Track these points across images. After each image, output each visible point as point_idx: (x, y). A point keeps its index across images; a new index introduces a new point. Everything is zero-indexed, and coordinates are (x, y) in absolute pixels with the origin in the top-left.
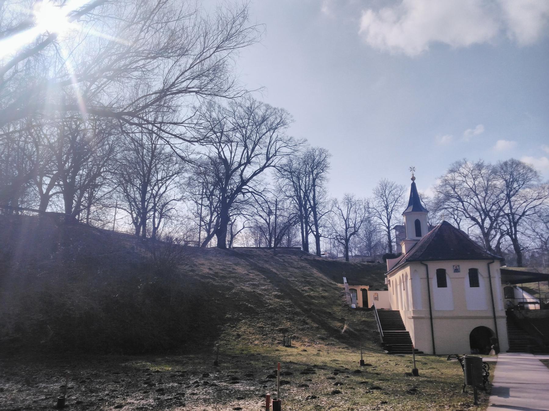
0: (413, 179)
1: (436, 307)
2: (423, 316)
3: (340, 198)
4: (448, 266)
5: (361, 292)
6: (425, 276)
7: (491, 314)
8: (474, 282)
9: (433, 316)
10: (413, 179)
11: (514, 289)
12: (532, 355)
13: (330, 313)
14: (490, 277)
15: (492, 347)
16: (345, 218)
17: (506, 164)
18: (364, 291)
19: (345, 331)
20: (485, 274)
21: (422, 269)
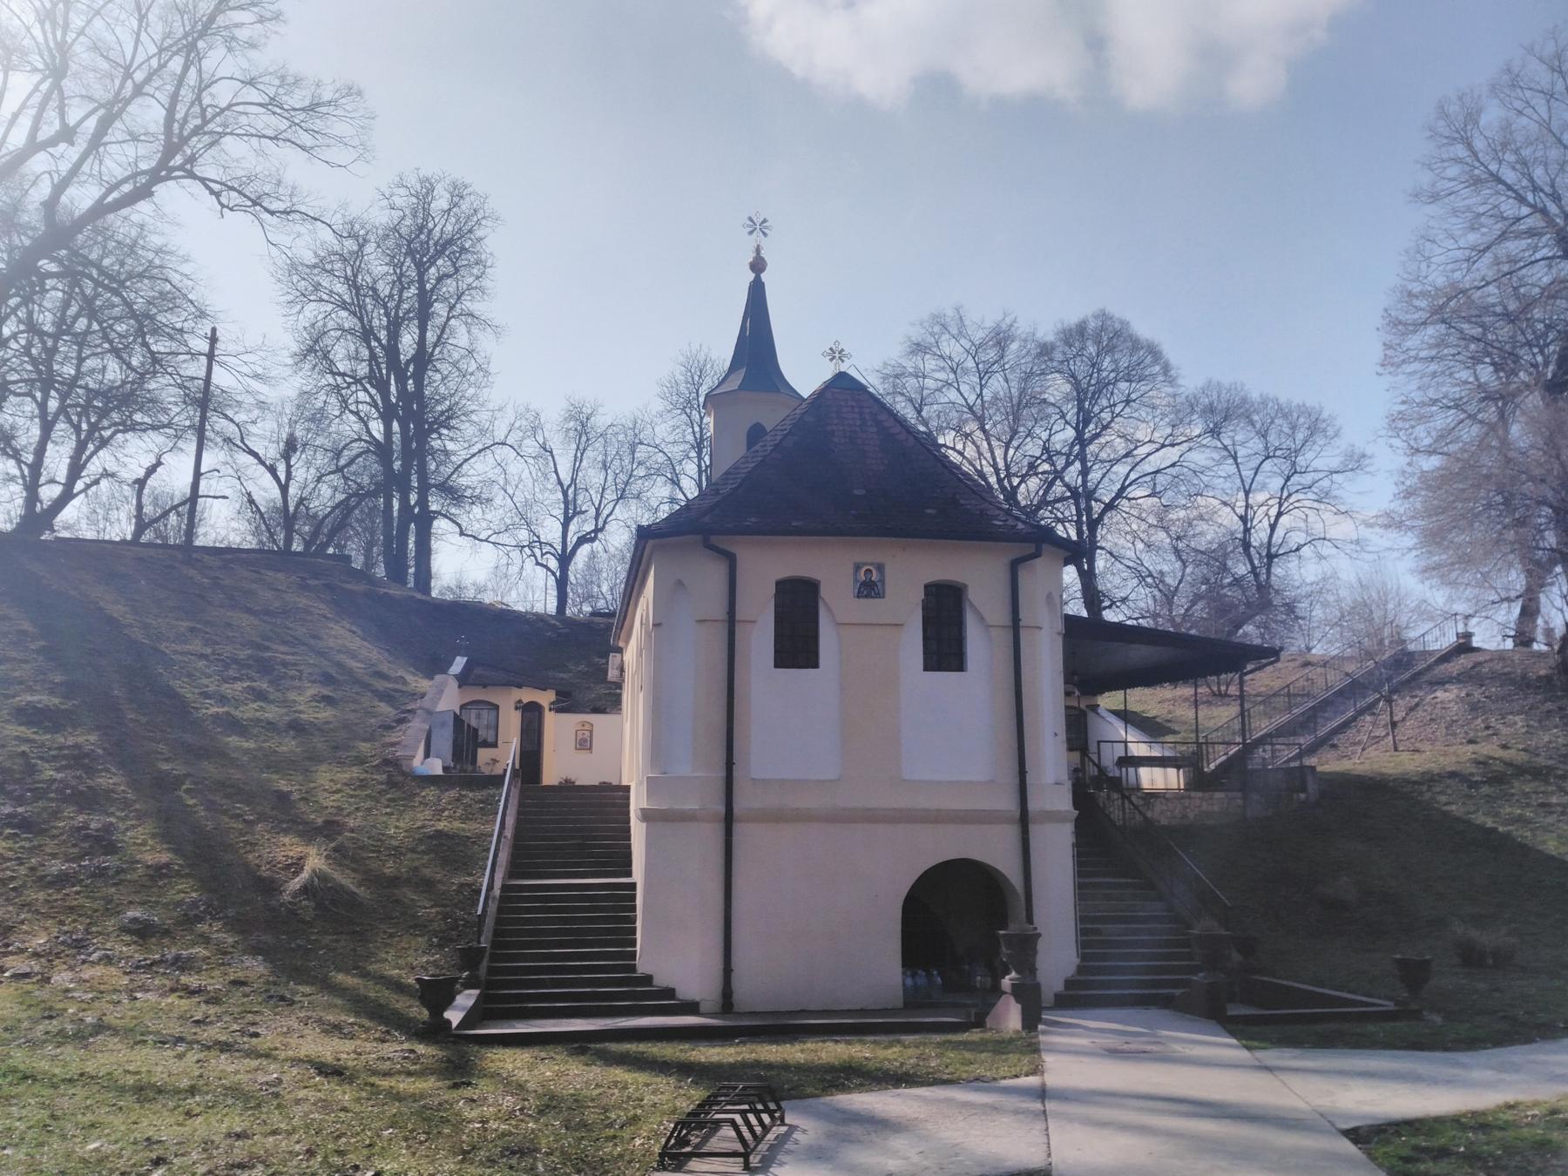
0: (758, 266)
1: (762, 758)
2: (692, 805)
3: (553, 414)
4: (831, 567)
5: (518, 714)
6: (720, 611)
7: (1006, 802)
8: (945, 651)
9: (738, 808)
10: (758, 266)
11: (1091, 715)
12: (1226, 1048)
13: (283, 797)
14: (1015, 625)
15: (1006, 982)
16: (566, 482)
17: (1081, 330)
18: (532, 713)
19: (306, 889)
20: (997, 614)
21: (707, 576)
